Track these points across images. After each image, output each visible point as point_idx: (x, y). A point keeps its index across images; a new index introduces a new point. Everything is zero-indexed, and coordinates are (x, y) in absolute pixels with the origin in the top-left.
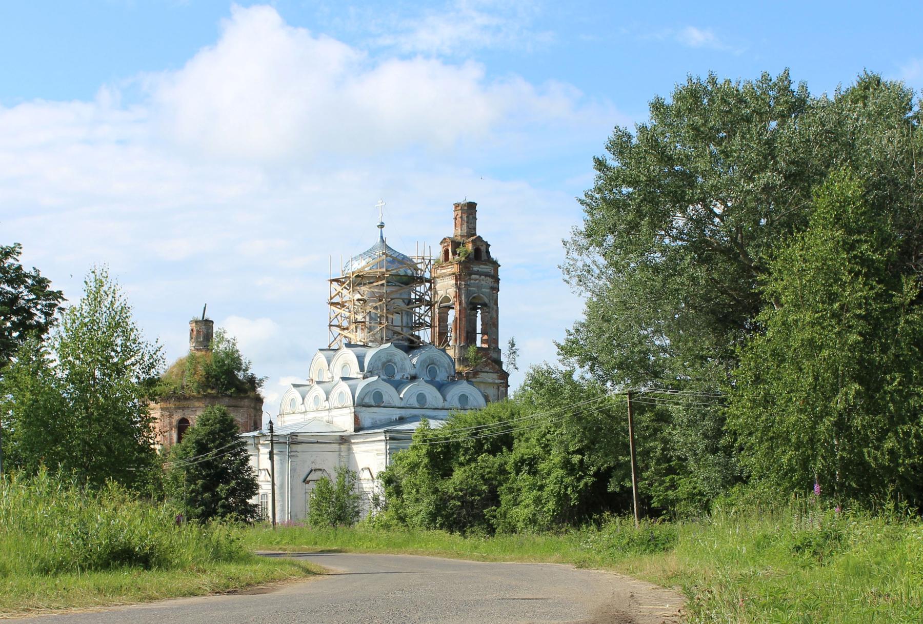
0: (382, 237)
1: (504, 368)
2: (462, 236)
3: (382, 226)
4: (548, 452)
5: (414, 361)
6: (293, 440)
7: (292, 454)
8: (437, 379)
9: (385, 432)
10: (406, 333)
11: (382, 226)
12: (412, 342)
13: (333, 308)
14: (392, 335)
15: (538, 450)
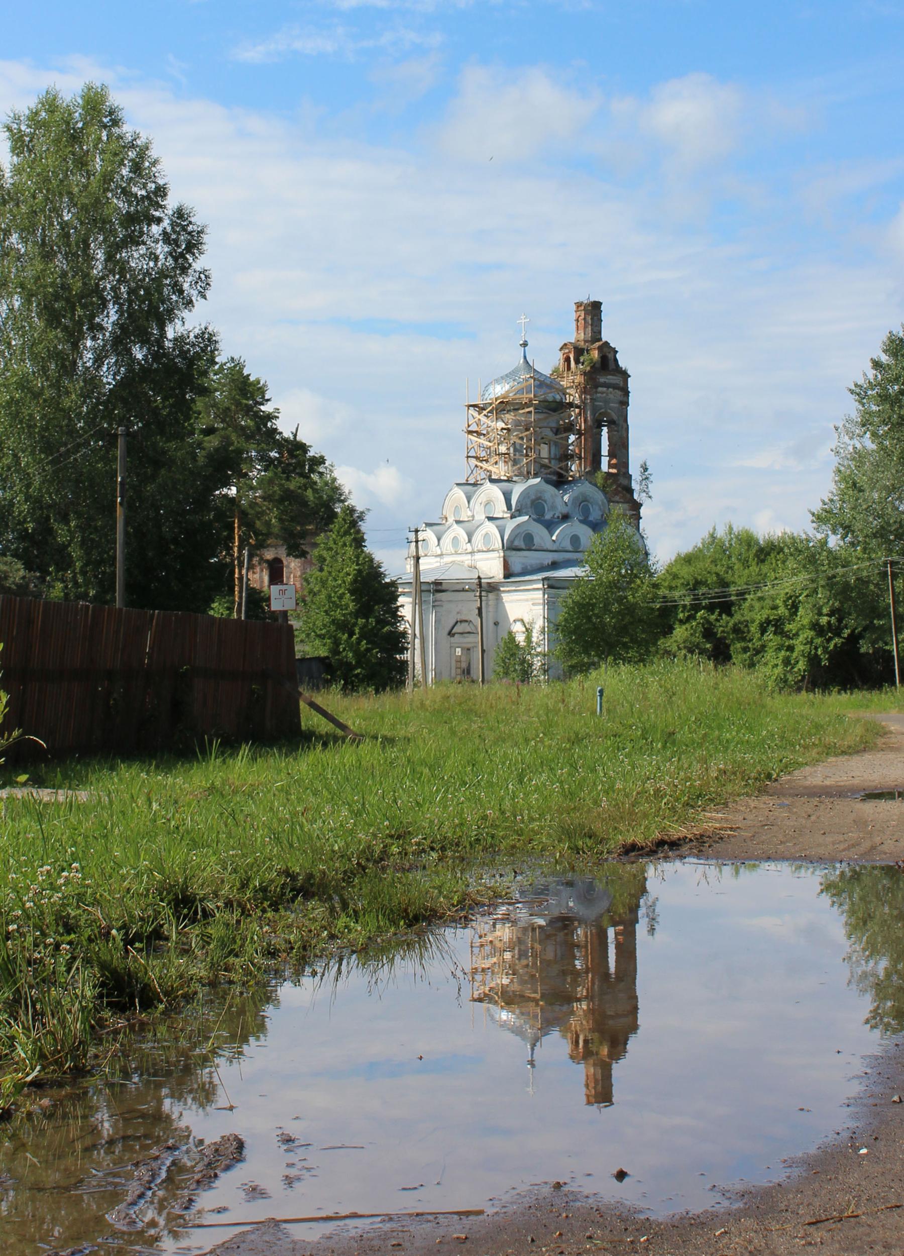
0: (525, 357)
1: (636, 496)
2: (585, 341)
3: (525, 345)
4: (795, 613)
5: (566, 498)
6: (438, 587)
7: (436, 604)
8: (591, 518)
9: (543, 579)
10: (555, 466)
11: (525, 345)
12: (560, 475)
13: (470, 436)
14: (540, 469)
15: (782, 611)
